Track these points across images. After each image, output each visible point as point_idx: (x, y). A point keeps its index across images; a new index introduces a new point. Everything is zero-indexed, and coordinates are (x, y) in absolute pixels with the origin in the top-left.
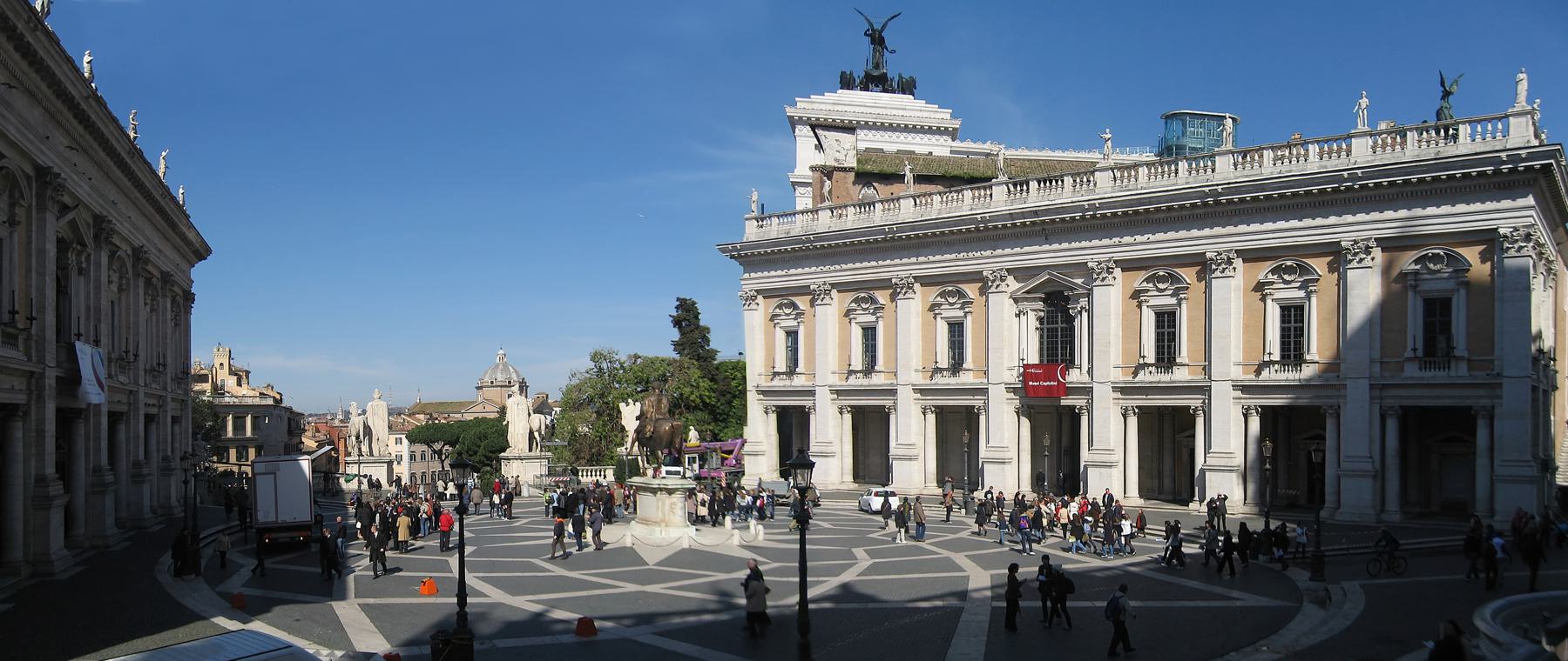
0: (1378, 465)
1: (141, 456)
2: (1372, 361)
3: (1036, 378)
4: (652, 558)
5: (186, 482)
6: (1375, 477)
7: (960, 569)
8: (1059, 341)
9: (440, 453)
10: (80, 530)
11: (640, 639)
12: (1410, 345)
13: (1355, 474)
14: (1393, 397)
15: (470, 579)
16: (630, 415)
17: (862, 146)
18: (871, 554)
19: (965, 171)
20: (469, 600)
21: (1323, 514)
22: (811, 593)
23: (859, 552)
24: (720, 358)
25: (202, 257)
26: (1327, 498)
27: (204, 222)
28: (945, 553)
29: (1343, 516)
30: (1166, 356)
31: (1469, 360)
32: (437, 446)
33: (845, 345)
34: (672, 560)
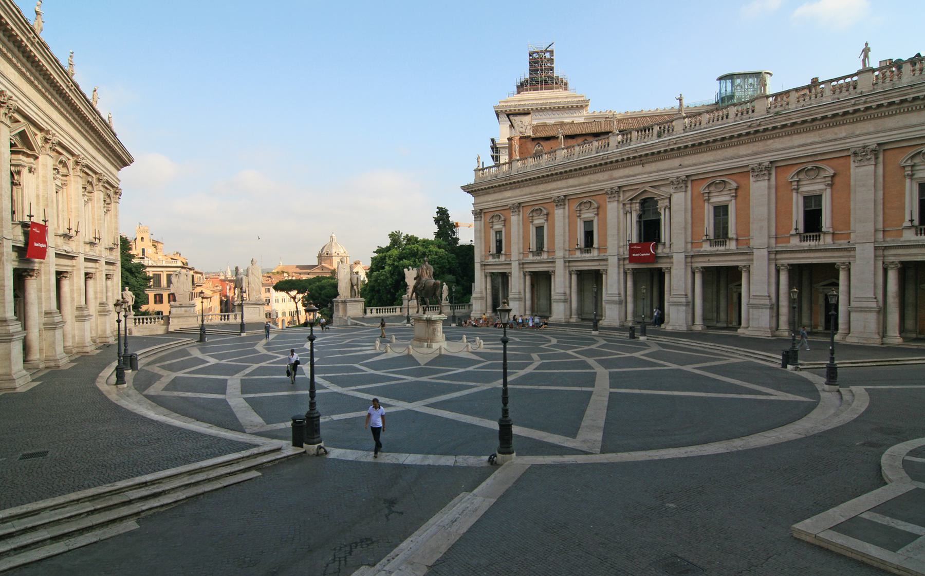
0: (881, 303)
1: (83, 303)
2: (876, 231)
3: (637, 251)
4: (422, 362)
5: (119, 321)
6: (878, 312)
7: (590, 367)
8: (650, 230)
9: (294, 298)
10: (35, 356)
11: (416, 409)
12: (907, 218)
13: (862, 310)
14: (895, 255)
15: (317, 379)
16: (410, 276)
17: (535, 123)
18: (542, 357)
19: (595, 130)
20: (317, 392)
21: (837, 338)
22: (509, 379)
23: (535, 356)
24: (460, 242)
25: (125, 164)
26: (840, 326)
27: (127, 136)
28: (583, 358)
29: (852, 340)
30: (721, 235)
31: (737, 240)
32: (294, 293)
33: (526, 237)
34: (433, 362)
